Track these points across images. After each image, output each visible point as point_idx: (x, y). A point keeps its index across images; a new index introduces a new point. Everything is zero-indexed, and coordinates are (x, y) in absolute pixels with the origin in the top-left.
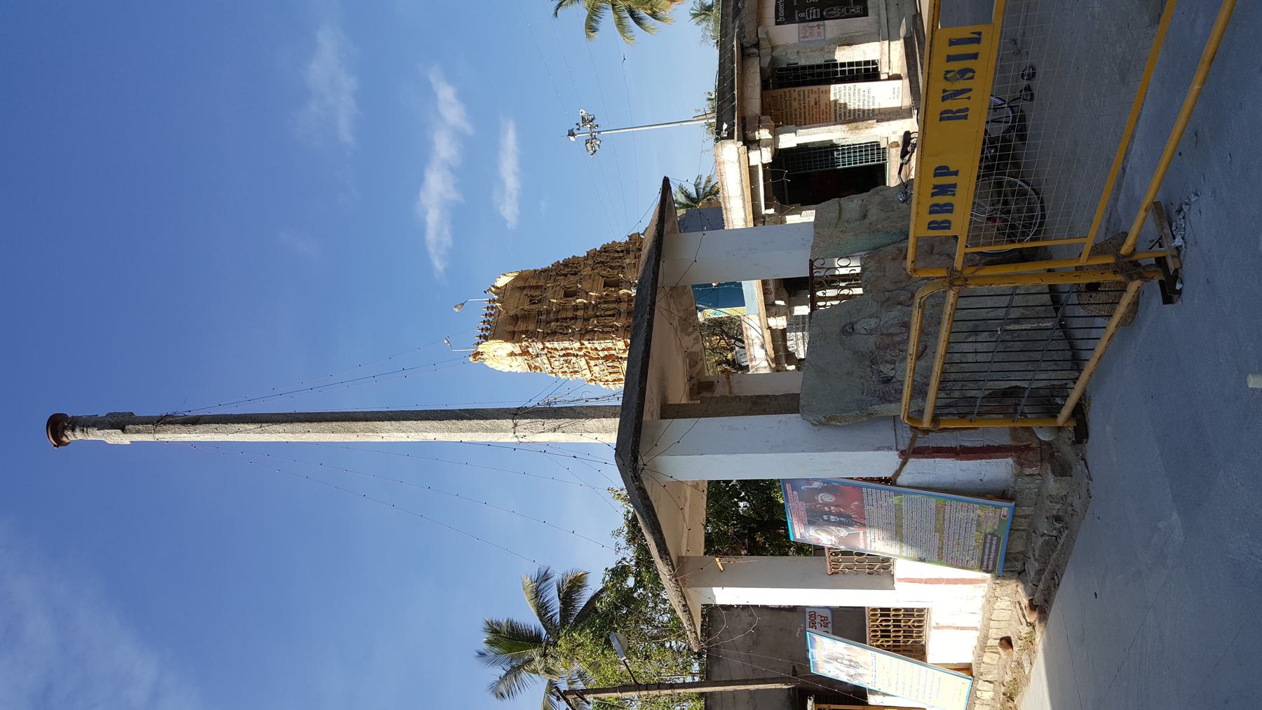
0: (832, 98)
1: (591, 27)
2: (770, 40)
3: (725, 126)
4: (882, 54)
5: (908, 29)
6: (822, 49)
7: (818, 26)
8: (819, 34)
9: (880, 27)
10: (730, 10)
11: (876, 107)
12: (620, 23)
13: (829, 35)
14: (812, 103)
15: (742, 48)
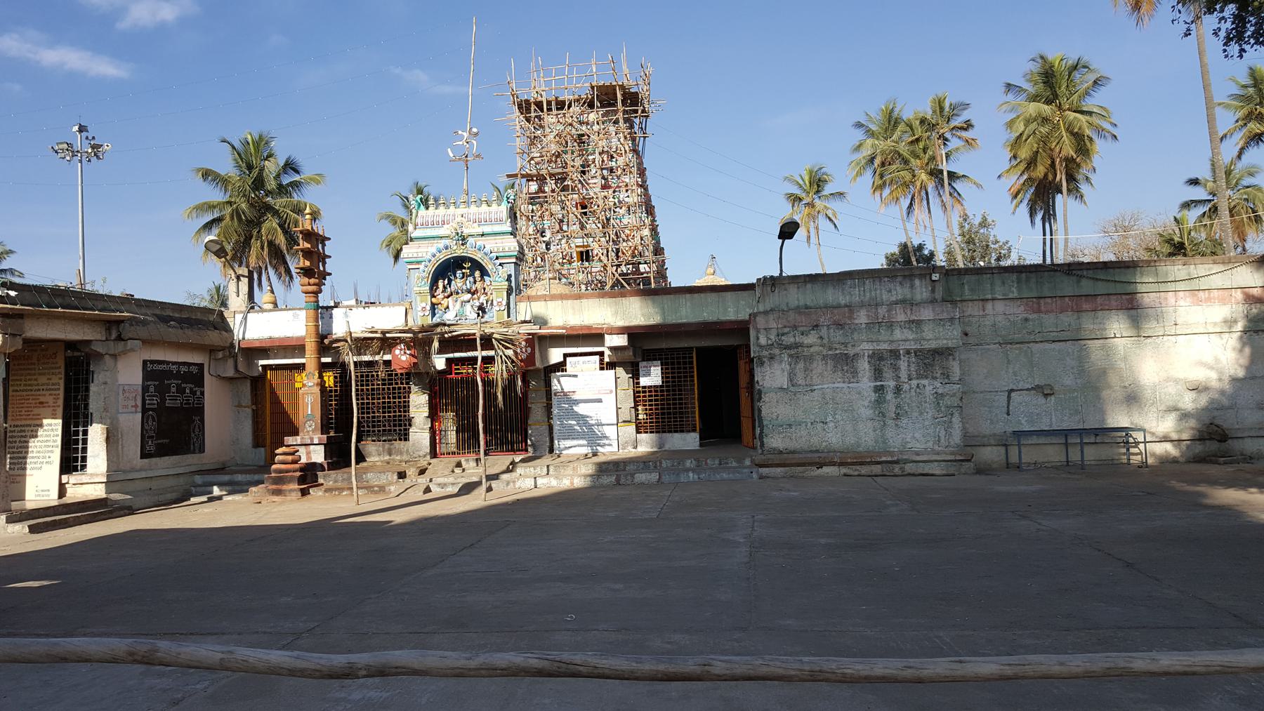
0: (45, 422)
1: (207, 174)
2: (125, 352)
3: (13, 293)
4: (92, 475)
5: (116, 502)
6: (106, 410)
7: (136, 406)
8: (126, 407)
9: (124, 472)
10: (169, 313)
11: (28, 472)
12: (211, 207)
13: (122, 418)
14: (42, 399)
15: (119, 322)
